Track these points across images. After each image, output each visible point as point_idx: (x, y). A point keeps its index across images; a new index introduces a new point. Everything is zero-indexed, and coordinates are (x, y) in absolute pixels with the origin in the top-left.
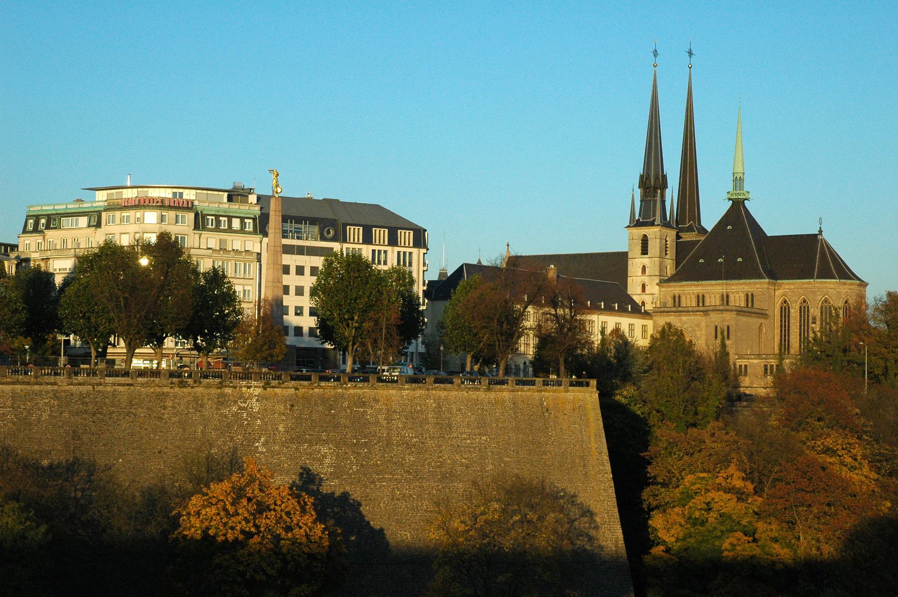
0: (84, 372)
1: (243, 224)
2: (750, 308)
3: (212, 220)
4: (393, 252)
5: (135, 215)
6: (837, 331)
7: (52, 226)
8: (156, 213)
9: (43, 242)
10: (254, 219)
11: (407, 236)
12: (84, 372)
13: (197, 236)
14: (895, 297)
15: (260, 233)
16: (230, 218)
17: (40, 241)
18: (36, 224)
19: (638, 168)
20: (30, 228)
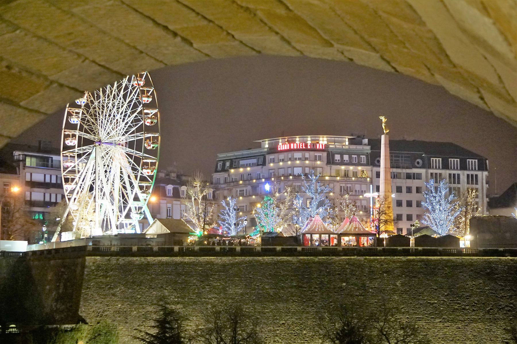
0: (333, 326)
1: (350, 158)
2: (121, 226)
3: (355, 157)
4: (464, 175)
5: (288, 156)
6: (298, 300)
7: (234, 166)
8: (301, 154)
9: (228, 178)
10: (367, 156)
11: (473, 162)
12: (333, 326)
13: (329, 168)
14: (3, 169)
15: (371, 164)
16: (359, 155)
17: (226, 176)
18: (224, 165)
19: (486, 99)
20: (219, 168)
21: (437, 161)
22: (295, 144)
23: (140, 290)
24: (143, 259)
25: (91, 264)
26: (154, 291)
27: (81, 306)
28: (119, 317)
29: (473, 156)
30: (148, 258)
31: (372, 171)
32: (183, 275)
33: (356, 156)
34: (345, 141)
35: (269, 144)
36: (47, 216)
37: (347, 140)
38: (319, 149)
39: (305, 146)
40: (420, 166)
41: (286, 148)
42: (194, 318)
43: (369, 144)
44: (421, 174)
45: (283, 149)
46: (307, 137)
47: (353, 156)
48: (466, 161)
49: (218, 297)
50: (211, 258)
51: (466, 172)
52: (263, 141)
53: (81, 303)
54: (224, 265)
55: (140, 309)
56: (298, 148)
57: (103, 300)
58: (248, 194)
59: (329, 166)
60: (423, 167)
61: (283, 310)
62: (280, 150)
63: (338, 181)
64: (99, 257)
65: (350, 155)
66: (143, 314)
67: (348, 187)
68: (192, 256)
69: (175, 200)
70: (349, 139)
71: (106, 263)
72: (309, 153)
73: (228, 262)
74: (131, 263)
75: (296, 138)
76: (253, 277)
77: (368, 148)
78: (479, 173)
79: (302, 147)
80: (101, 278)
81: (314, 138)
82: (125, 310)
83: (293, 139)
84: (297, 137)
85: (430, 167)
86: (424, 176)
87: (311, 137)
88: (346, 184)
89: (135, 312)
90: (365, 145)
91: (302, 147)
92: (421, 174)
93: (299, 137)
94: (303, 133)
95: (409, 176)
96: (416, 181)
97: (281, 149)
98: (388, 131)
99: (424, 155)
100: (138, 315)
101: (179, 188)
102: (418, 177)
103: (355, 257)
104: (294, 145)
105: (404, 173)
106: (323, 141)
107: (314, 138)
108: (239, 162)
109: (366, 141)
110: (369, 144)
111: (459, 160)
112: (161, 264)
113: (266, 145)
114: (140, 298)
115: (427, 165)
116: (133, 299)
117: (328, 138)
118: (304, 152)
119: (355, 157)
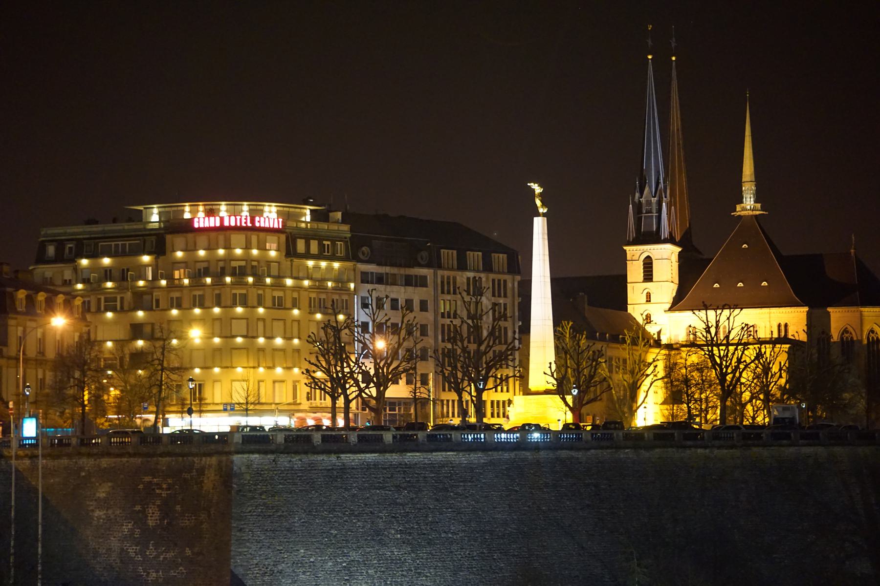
3: (328, 245)
7: (85, 253)
13: (289, 263)
21: (449, 255)
22: (218, 219)
23: (335, 519)
24: (333, 458)
25: (243, 469)
26: (359, 521)
27: (232, 553)
28: (304, 573)
29: (501, 248)
30: (343, 456)
31: (354, 270)
32: (405, 489)
33: (329, 243)
34: (305, 215)
35: (160, 214)
36: (13, 362)
37: (308, 212)
38: (273, 227)
39: (251, 223)
40: (367, 259)
41: (212, 225)
42: (431, 570)
43: (344, 221)
44: (425, 277)
45: (207, 225)
46: (242, 205)
47: (324, 242)
48: (440, 252)
49: (467, 529)
50: (448, 453)
51: (492, 276)
52: (145, 208)
53: (233, 548)
54: (470, 468)
55: (338, 556)
56: (238, 224)
57: (271, 540)
58: (126, 308)
59: (290, 259)
60: (428, 266)
61: (574, 551)
62: (199, 228)
63: (306, 289)
64: (257, 455)
65: (320, 240)
66: (345, 567)
67: (343, 300)
68: (418, 451)
69: (30, 320)
70: (311, 211)
71: (270, 466)
72: (258, 236)
73: (476, 461)
74: (312, 466)
75: (220, 205)
76: (520, 489)
77: (346, 228)
78: (508, 278)
79: (246, 223)
80: (263, 497)
81: (254, 207)
82: (312, 560)
83: (259, 207)
84: (187, 204)
85: (440, 267)
86: (430, 280)
87: (204, 205)
88: (340, 294)
89: (331, 564)
90: (337, 222)
91: (246, 223)
92: (425, 277)
93: (190, 205)
94: (234, 196)
95: (409, 281)
96: (420, 290)
97: (202, 225)
98: (545, 210)
99: (429, 244)
100: (336, 569)
101: (34, 296)
102: (421, 282)
103: (410, 434)
104: (236, 219)
105: (401, 275)
106: (270, 212)
107: (254, 207)
108: (96, 245)
109: (339, 215)
110: (344, 221)
111: (480, 253)
112: (368, 467)
113: (154, 215)
114: (336, 534)
115: (435, 263)
116: (323, 538)
117: (251, 207)
118: (249, 233)
119: (328, 245)
